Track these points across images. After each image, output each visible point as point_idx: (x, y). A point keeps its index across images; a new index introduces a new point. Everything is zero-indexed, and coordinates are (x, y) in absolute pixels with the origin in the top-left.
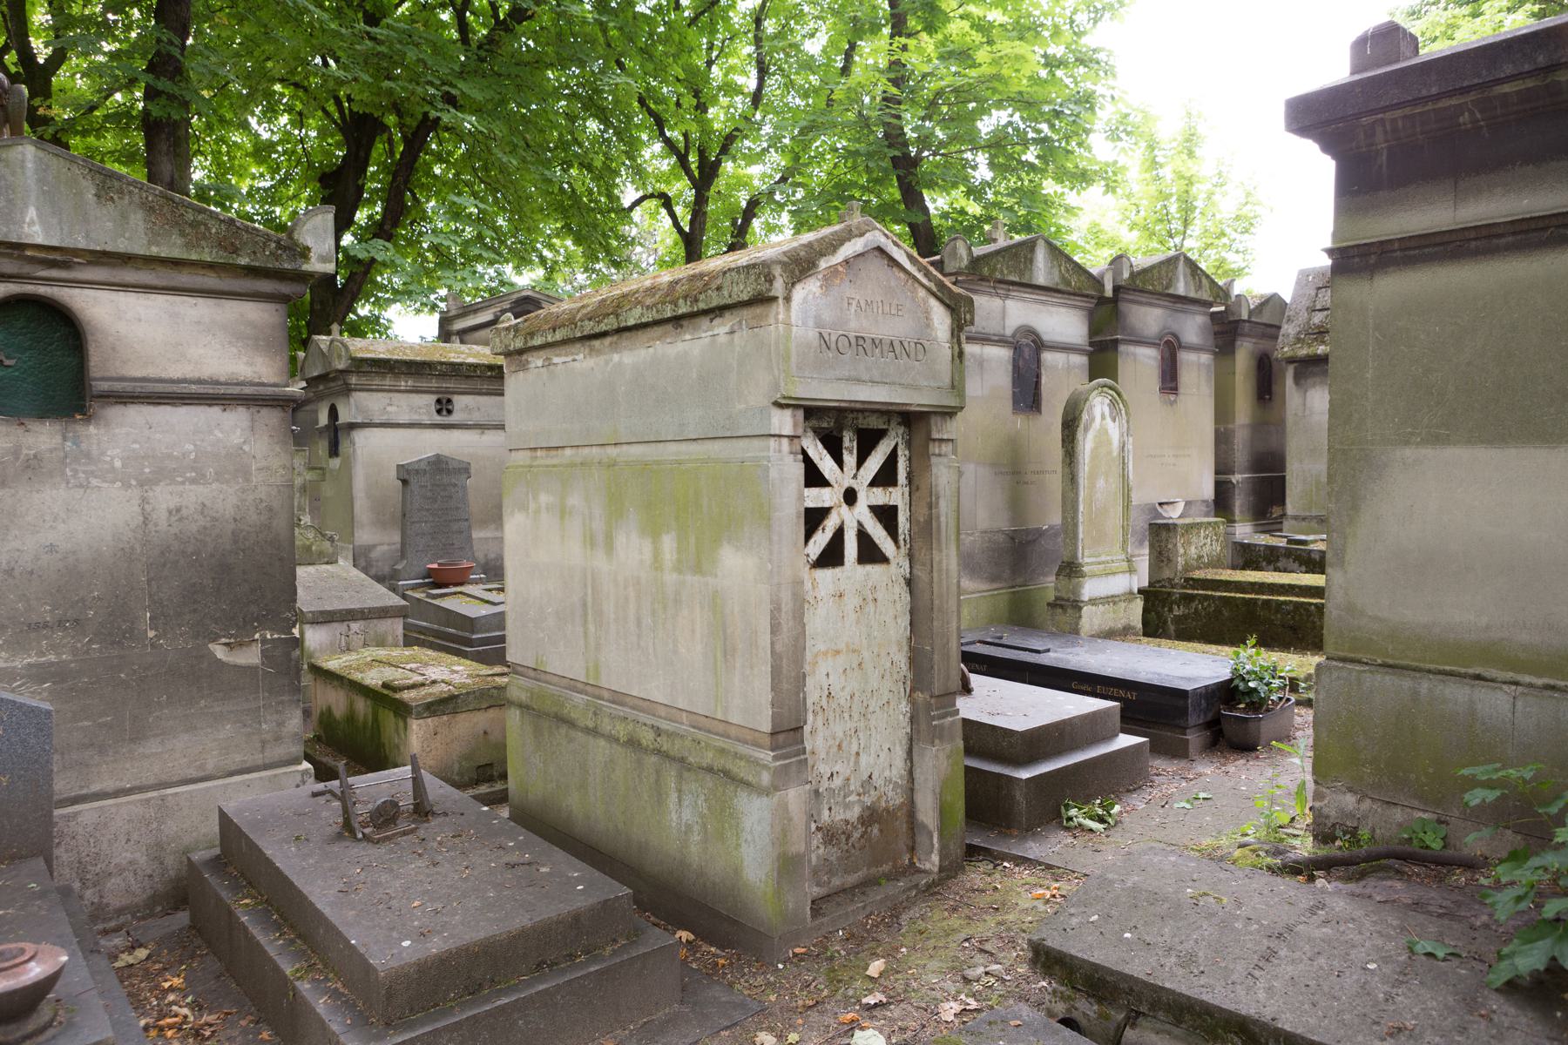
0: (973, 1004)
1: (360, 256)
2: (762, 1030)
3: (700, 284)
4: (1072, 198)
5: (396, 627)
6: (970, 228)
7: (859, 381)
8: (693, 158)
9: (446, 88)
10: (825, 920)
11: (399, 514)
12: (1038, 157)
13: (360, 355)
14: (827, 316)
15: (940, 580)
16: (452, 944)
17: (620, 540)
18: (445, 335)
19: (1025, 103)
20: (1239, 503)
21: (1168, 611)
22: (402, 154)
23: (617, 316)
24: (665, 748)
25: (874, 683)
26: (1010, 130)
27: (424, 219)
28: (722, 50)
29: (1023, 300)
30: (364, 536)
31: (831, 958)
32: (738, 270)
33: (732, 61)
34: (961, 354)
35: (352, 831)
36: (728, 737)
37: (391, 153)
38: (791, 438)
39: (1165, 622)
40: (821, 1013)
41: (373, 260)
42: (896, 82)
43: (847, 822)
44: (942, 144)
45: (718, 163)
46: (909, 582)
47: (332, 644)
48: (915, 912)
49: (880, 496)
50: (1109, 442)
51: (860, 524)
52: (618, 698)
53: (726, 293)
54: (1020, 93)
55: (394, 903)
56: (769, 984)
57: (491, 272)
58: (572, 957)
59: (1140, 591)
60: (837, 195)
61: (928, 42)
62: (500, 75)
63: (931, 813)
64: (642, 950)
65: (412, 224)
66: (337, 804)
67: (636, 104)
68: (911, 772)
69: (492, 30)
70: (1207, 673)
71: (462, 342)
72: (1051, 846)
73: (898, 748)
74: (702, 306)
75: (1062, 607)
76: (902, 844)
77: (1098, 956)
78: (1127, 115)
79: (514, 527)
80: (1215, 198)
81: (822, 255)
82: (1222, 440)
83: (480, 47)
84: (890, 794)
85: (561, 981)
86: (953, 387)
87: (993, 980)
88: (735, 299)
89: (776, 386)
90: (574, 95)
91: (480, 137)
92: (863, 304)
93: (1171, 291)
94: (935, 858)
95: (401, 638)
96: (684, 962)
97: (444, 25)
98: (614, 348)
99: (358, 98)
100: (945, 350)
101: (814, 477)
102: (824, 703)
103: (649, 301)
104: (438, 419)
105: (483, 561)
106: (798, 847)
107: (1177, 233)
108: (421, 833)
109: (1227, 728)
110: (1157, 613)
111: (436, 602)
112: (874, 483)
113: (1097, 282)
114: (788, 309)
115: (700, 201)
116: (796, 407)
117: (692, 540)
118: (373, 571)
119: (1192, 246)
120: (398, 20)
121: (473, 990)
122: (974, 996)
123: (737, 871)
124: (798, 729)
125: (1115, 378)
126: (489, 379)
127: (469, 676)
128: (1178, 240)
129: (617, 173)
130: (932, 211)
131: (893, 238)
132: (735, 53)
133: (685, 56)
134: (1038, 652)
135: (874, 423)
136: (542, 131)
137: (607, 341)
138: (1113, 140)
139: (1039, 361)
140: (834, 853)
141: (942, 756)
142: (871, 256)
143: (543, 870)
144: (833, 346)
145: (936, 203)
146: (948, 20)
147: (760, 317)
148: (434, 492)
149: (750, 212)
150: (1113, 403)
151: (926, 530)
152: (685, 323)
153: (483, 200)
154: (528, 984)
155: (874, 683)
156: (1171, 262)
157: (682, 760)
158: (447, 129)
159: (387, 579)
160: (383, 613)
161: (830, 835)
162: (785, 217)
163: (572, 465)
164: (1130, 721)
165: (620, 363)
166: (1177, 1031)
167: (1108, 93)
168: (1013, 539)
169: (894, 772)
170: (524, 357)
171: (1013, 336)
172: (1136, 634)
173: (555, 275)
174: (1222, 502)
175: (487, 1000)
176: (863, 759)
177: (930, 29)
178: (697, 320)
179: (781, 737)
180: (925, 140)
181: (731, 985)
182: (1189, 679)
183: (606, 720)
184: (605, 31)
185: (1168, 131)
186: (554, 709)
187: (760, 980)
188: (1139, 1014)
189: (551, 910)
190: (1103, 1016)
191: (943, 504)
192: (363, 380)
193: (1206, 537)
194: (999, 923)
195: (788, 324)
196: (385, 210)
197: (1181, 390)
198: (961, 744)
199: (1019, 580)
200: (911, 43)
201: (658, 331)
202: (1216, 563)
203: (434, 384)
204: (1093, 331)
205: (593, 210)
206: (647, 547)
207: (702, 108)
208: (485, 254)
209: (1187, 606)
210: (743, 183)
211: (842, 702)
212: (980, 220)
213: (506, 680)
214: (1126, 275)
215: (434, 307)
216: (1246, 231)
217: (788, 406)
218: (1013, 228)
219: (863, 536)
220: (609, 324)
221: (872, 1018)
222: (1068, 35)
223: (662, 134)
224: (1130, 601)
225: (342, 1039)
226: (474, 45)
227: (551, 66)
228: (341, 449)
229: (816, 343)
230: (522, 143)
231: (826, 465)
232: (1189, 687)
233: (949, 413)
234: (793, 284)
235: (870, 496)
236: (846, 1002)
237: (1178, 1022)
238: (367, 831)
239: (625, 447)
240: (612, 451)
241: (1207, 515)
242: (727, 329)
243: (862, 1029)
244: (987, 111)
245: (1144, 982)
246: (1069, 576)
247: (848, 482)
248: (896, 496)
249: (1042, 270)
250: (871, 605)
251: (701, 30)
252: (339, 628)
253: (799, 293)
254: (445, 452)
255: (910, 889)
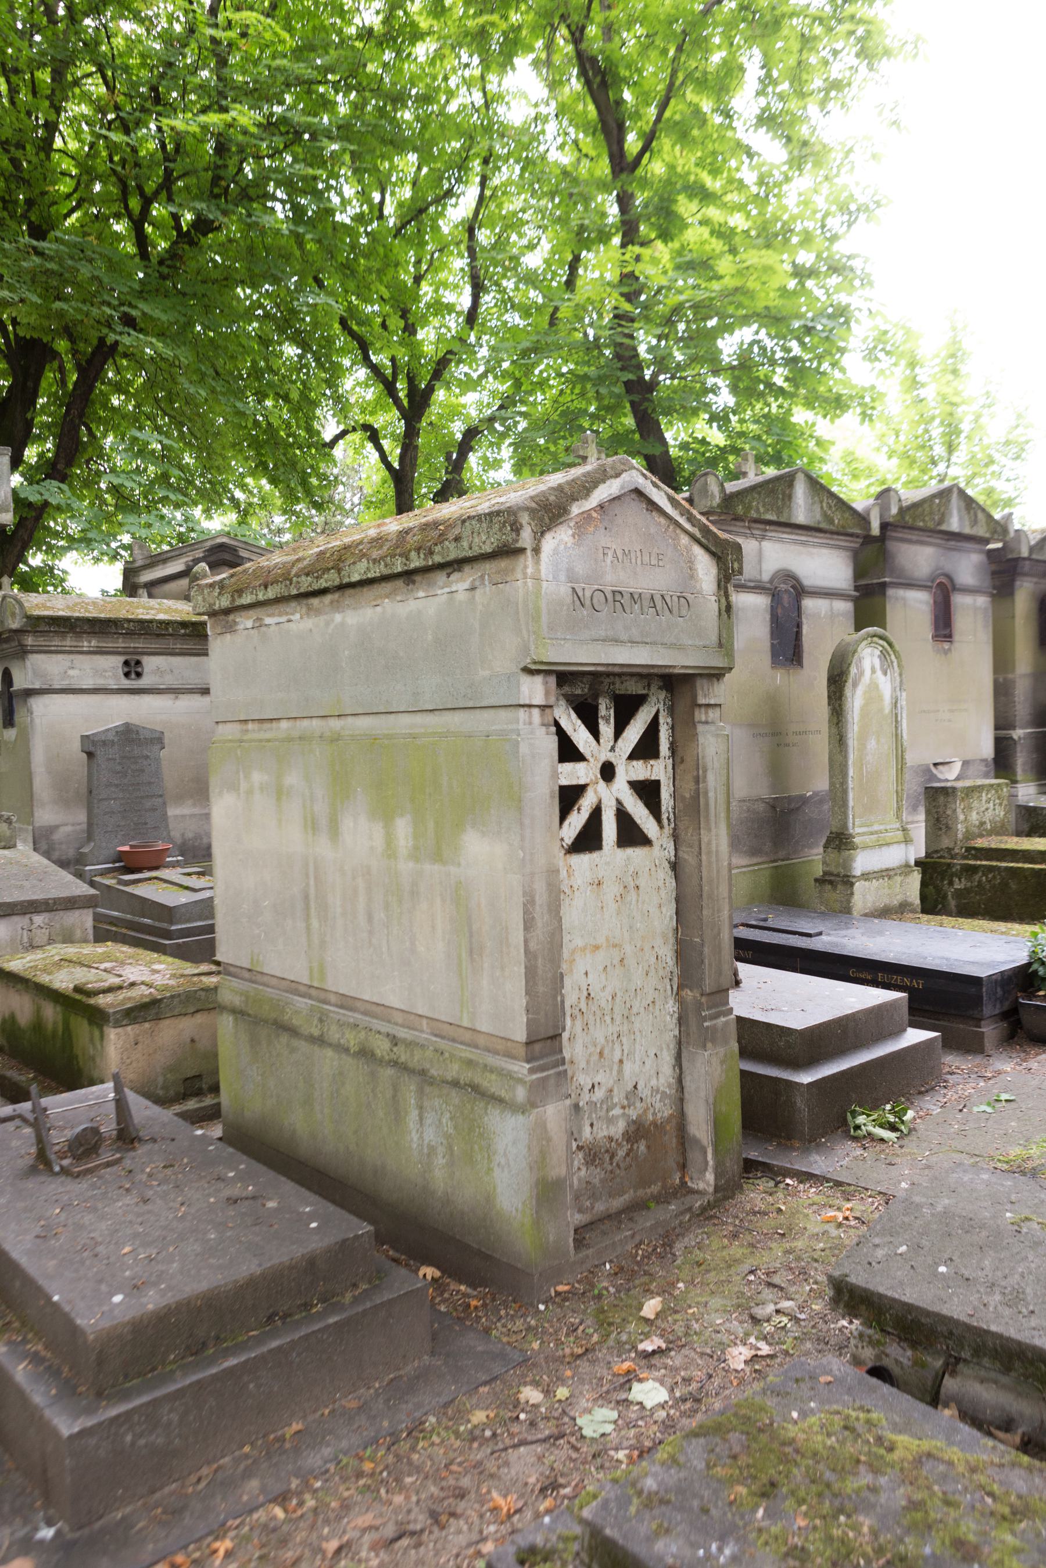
0: (765, 1349)
1: (31, 499)
2: (525, 1384)
3: (435, 534)
4: (823, 427)
5: (85, 919)
6: (713, 460)
7: (616, 641)
8: (401, 385)
9: (125, 309)
10: (590, 1252)
11: (84, 790)
12: (787, 379)
13: (36, 613)
14: (580, 569)
15: (710, 863)
16: (170, 1299)
17: (347, 824)
18: (130, 586)
19: (774, 320)
20: (1021, 760)
21: (950, 885)
22: (76, 383)
23: (339, 571)
24: (403, 1059)
25: (638, 980)
26: (756, 349)
27: (101, 456)
28: (431, 264)
29: (781, 541)
30: (46, 816)
31: (600, 1296)
32: (479, 518)
33: (442, 275)
34: (729, 608)
35: (48, 1164)
36: (476, 1047)
37: (63, 382)
38: (543, 708)
39: (945, 897)
40: (593, 1362)
41: (46, 504)
42: (629, 297)
43: (611, 1139)
44: (679, 367)
45: (430, 390)
46: (675, 866)
47: (13, 940)
48: (690, 1240)
49: (640, 771)
50: (881, 698)
51: (619, 802)
52: (347, 1003)
53: (465, 544)
54: (767, 308)
55: (100, 1249)
56: (529, 1329)
57: (178, 515)
58: (307, 1306)
59: (918, 863)
60: (567, 422)
61: (662, 251)
62: (184, 294)
63: (705, 1127)
64: (387, 1296)
65: (88, 462)
66: (28, 1131)
67: (337, 326)
68: (680, 1081)
69: (174, 243)
70: (1000, 957)
71: (150, 596)
72: (838, 1160)
73: (665, 1053)
74: (438, 559)
75: (831, 882)
76: (671, 1161)
77: (909, 1296)
78: (885, 332)
79: (224, 811)
80: (983, 421)
81: (574, 499)
82: (1002, 691)
83: (161, 262)
84: (658, 1105)
85: (296, 1336)
86: (720, 645)
87: (785, 1320)
88: (476, 551)
89: (526, 650)
90: (267, 315)
91: (163, 365)
92: (619, 553)
93: (944, 527)
94: (710, 1176)
95: (91, 931)
96: (433, 1305)
97: (118, 237)
98: (336, 606)
99: (25, 321)
100: (711, 605)
101: (568, 752)
102: (583, 1005)
103: (375, 554)
104: (126, 683)
105: (179, 841)
106: (558, 1170)
107: (941, 458)
108: (127, 1163)
109: (1025, 1017)
110: (936, 887)
111: (128, 889)
112: (633, 756)
113: (862, 519)
114: (537, 562)
115: (411, 433)
116: (547, 673)
117: (431, 825)
118: (56, 855)
119: (957, 472)
120: (67, 232)
121: (197, 1350)
122: (765, 1338)
123: (490, 1199)
124: (556, 1037)
125: (883, 626)
126: (190, 637)
127: (173, 976)
128: (941, 467)
129: (315, 404)
130: (671, 442)
131: (636, 475)
132: (445, 266)
133: (391, 272)
134: (809, 935)
135: (633, 688)
136: (233, 358)
137: (328, 598)
138: (870, 360)
139: (799, 609)
140: (597, 1175)
141: (715, 1061)
142: (627, 499)
143: (271, 1204)
144: (588, 603)
145: (675, 434)
146: (686, 226)
147: (506, 572)
148: (122, 764)
149: (466, 446)
150: (884, 655)
151: (692, 808)
152: (418, 578)
153: (168, 435)
154: (260, 1341)
155: (638, 980)
156: (944, 494)
157: (423, 1073)
158: (125, 355)
159: (74, 864)
160: (71, 904)
161: (592, 1155)
162: (506, 452)
163: (290, 740)
164: (920, 1011)
165: (343, 624)
166: (1004, 1380)
167: (865, 306)
168: (774, 807)
169: (662, 1080)
170: (231, 617)
171: (771, 581)
172: (914, 911)
173: (249, 519)
174: (1002, 761)
175: (212, 1361)
176: (628, 1067)
177: (665, 236)
178: (431, 575)
179: (537, 1047)
180: (662, 362)
181: (487, 1331)
182: (981, 964)
183: (334, 1028)
184: (301, 244)
185: (930, 348)
186: (273, 1015)
187: (519, 1324)
188: (958, 1360)
189: (284, 1254)
190: (918, 1363)
191: (711, 777)
192: (41, 641)
193: (988, 801)
194: (788, 1252)
195: (537, 579)
196: (58, 447)
197: (956, 637)
198: (735, 1046)
199: (782, 854)
200: (646, 252)
201: (387, 587)
202: (999, 830)
203: (121, 643)
204: (859, 573)
205: (291, 445)
206: (378, 831)
207: (410, 329)
208: (172, 497)
209: (969, 878)
210: (454, 412)
211: (603, 1004)
212: (723, 450)
213: (214, 979)
214: (894, 510)
215: (115, 557)
216: (1017, 458)
217: (538, 672)
218: (760, 460)
219: (623, 817)
220: (330, 579)
221: (650, 1367)
222: (820, 243)
223: (366, 359)
224: (907, 874)
225: (48, 1413)
226: (154, 260)
227: (243, 283)
228: (17, 718)
229: (568, 600)
230: (211, 372)
231: (581, 736)
232: (983, 973)
233: (716, 675)
234: (543, 533)
235: (629, 771)
236: (621, 1349)
237: (1007, 1369)
238: (65, 1162)
239: (350, 719)
240: (335, 724)
241: (986, 776)
242: (466, 585)
243: (640, 1381)
244: (730, 329)
245: (965, 1324)
246: (839, 848)
247: (605, 755)
248: (658, 770)
249: (802, 507)
250: (633, 893)
251: (409, 241)
252: (20, 922)
253: (549, 543)
254: (135, 720)
255: (682, 1213)
